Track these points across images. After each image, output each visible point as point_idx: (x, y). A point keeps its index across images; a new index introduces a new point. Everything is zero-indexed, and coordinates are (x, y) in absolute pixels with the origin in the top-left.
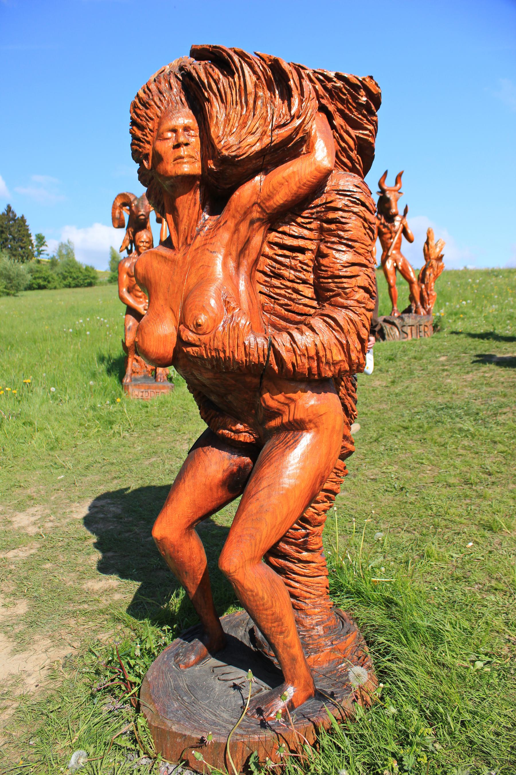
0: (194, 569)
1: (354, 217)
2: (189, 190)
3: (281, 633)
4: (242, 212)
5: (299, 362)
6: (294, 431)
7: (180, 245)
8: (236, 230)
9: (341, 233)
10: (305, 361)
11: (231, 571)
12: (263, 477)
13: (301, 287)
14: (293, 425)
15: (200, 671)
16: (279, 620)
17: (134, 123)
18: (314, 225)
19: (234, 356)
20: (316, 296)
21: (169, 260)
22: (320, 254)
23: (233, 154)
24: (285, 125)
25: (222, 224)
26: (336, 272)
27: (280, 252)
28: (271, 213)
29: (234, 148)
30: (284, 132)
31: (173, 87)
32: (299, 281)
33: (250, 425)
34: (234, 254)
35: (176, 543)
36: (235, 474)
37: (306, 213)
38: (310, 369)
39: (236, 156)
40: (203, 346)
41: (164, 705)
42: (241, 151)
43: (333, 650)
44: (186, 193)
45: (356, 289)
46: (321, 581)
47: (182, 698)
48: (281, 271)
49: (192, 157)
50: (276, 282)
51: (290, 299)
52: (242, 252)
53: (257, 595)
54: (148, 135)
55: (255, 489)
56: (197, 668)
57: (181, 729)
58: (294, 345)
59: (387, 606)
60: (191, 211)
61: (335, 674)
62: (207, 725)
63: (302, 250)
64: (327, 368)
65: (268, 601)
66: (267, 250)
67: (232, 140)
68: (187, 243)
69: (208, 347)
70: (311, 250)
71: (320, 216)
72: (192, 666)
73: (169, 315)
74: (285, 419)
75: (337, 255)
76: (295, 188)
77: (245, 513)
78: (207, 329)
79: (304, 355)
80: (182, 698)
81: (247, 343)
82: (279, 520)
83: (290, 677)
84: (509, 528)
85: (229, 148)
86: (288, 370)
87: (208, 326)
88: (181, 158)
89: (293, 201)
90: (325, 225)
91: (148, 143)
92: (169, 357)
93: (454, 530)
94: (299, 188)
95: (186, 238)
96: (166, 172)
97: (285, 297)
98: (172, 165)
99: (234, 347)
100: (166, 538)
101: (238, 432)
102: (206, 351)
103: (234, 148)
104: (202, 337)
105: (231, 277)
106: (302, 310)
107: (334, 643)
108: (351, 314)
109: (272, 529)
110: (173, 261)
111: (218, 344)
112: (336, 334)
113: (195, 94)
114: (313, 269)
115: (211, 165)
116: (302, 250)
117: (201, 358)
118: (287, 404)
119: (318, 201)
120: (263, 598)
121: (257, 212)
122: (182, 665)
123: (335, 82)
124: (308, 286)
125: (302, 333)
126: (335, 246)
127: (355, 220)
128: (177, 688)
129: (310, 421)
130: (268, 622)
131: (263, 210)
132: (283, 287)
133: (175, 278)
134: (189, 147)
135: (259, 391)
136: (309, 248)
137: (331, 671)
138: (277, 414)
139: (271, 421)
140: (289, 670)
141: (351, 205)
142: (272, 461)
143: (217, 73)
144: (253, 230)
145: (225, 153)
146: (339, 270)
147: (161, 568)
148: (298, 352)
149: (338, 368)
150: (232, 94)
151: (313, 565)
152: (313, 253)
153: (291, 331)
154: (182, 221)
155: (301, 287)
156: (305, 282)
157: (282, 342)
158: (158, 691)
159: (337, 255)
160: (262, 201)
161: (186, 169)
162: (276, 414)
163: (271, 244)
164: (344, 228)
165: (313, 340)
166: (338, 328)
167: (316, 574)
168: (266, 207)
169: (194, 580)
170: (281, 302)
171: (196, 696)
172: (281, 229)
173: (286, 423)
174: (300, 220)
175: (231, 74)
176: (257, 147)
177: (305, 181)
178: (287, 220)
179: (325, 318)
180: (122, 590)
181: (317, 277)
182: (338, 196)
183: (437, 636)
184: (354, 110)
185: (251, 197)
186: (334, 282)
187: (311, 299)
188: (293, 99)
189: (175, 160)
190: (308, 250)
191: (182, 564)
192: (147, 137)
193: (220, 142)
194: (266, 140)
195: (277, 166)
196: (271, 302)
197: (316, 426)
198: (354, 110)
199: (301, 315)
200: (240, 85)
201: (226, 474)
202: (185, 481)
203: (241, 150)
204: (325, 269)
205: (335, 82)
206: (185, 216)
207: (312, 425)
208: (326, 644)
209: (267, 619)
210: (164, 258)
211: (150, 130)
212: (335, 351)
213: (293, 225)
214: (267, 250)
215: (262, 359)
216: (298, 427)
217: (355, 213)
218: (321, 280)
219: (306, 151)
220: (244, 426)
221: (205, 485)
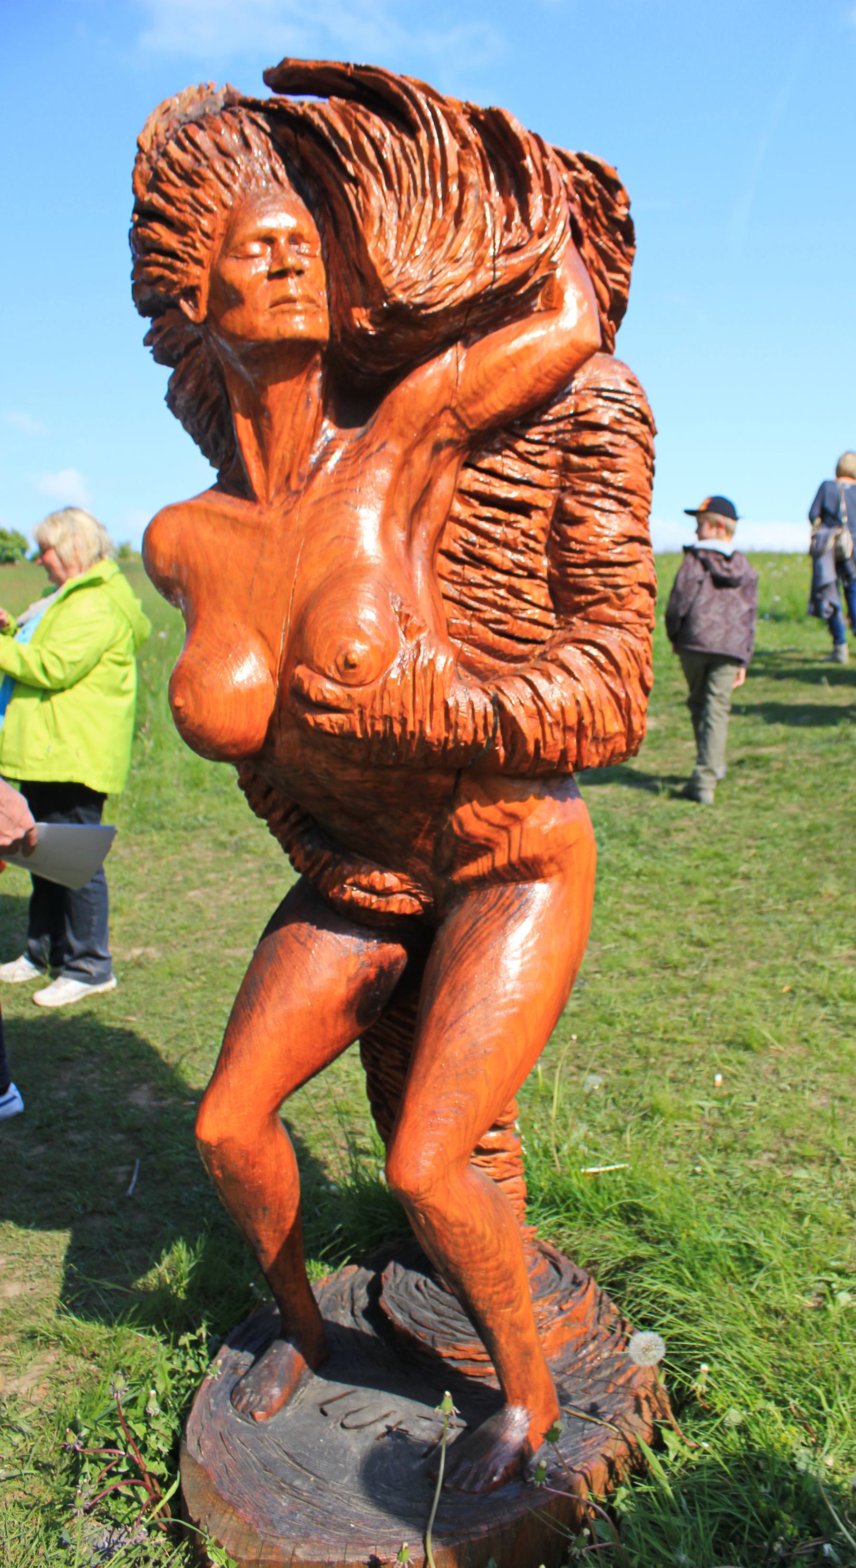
0: (281, 1199)
1: (632, 445)
2: (299, 372)
3: (509, 1302)
4: (420, 425)
5: (549, 738)
6: (517, 882)
7: (272, 493)
8: (405, 463)
9: (606, 474)
10: (558, 735)
11: (422, 1189)
12: (468, 983)
13: (524, 585)
14: (517, 870)
15: (296, 1416)
16: (507, 1277)
17: (145, 213)
18: (553, 456)
19: (422, 731)
20: (554, 602)
21: (244, 525)
22: (562, 517)
23: (418, 300)
24: (518, 248)
25: (374, 448)
26: (603, 554)
27: (487, 512)
28: (475, 430)
29: (421, 289)
30: (518, 261)
31: (253, 144)
32: (520, 572)
33: (416, 878)
34: (402, 514)
35: (250, 1148)
36: (372, 983)
37: (535, 434)
38: (564, 753)
39: (425, 306)
40: (356, 711)
41: (258, 1508)
42: (435, 296)
43: (567, 1322)
44: (292, 378)
45: (637, 589)
46: (516, 1187)
47: (291, 1485)
48: (486, 552)
49: (312, 301)
50: (473, 575)
51: (505, 609)
52: (416, 512)
53: (473, 1231)
54: (198, 245)
55: (453, 1011)
56: (289, 1412)
57: (316, 1551)
58: (541, 704)
59: (629, 1221)
60: (298, 419)
61: (582, 1369)
62: (368, 1530)
63: (523, 508)
64: (593, 750)
65: (491, 1242)
66: (458, 508)
67: (415, 271)
68: (289, 488)
69: (367, 712)
70: (543, 509)
71: (563, 440)
72: (278, 1410)
73: (255, 646)
74: (501, 859)
75: (603, 520)
76: (530, 380)
77: (438, 1063)
78: (368, 673)
79: (557, 724)
80: (291, 1485)
81: (451, 702)
82: (511, 1067)
83: (518, 1391)
84: (779, 1040)
85: (409, 287)
86: (526, 754)
87: (370, 667)
88: (291, 300)
89: (522, 406)
90: (575, 459)
91: (198, 262)
92: (257, 738)
93: (681, 1057)
94: (538, 380)
95: (288, 478)
96: (253, 329)
97: (494, 605)
98: (267, 316)
99: (424, 710)
100: (230, 1139)
101: (387, 892)
102: (362, 720)
103: (421, 289)
104: (357, 692)
105: (398, 561)
106: (528, 631)
107: (565, 1307)
108: (629, 638)
109: (497, 1089)
110: (258, 528)
111: (392, 706)
112: (608, 679)
113: (315, 168)
114: (547, 548)
115: (361, 318)
116: (523, 508)
117: (351, 735)
118: (505, 828)
119: (557, 410)
120: (484, 1236)
121: (449, 426)
122: (259, 1414)
123: (579, 172)
124: (538, 582)
125: (549, 678)
126: (598, 502)
127: (634, 451)
128: (267, 1465)
129: (552, 859)
130: (486, 1285)
131: (461, 423)
132: (488, 584)
133: (266, 564)
134: (303, 277)
135: (451, 801)
136: (540, 504)
137: (570, 1365)
138: (485, 848)
139: (466, 864)
140: (518, 1378)
141: (627, 419)
142: (482, 948)
143: (376, 125)
144: (439, 463)
145: (401, 297)
146: (608, 550)
147: (93, 1212)
148: (549, 719)
149: (610, 747)
150: (411, 171)
151: (502, 1156)
152: (546, 515)
153: (529, 676)
154: (278, 440)
155: (524, 585)
156: (532, 574)
157: (516, 698)
158: (232, 1481)
159: (603, 520)
160: (460, 404)
161: (301, 327)
162: (482, 848)
163: (465, 494)
164: (614, 465)
165: (560, 690)
166: (611, 668)
167: (506, 1175)
168: (469, 417)
169: (278, 1222)
170: (487, 616)
171: (319, 1473)
172: (485, 464)
173: (503, 866)
174: (521, 446)
175: (412, 130)
176: (466, 290)
177: (550, 366)
178: (498, 446)
179: (587, 648)
180: (19, 1273)
181: (560, 564)
182: (600, 402)
183: (749, 1260)
184: (602, 231)
185: (440, 393)
186: (597, 575)
187: (545, 609)
188: (531, 197)
189: (275, 304)
190: (537, 508)
191: (261, 1191)
192: (195, 248)
193: (390, 272)
194: (483, 277)
195: (485, 333)
196: (465, 617)
197: (561, 870)
198: (602, 231)
199: (526, 641)
200: (432, 156)
201: (354, 985)
202: (263, 1010)
203: (434, 294)
204: (578, 547)
205: (579, 172)
206: (286, 430)
207: (553, 868)
208: (551, 1312)
209: (486, 1279)
210: (235, 522)
211: (205, 234)
212: (609, 714)
213: (507, 456)
214: (458, 508)
215: (481, 735)
216: (528, 870)
217: (632, 437)
218: (570, 570)
219: (543, 304)
220: (402, 881)
221: (311, 1013)
